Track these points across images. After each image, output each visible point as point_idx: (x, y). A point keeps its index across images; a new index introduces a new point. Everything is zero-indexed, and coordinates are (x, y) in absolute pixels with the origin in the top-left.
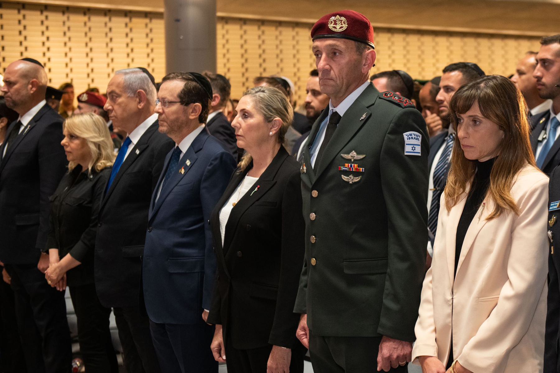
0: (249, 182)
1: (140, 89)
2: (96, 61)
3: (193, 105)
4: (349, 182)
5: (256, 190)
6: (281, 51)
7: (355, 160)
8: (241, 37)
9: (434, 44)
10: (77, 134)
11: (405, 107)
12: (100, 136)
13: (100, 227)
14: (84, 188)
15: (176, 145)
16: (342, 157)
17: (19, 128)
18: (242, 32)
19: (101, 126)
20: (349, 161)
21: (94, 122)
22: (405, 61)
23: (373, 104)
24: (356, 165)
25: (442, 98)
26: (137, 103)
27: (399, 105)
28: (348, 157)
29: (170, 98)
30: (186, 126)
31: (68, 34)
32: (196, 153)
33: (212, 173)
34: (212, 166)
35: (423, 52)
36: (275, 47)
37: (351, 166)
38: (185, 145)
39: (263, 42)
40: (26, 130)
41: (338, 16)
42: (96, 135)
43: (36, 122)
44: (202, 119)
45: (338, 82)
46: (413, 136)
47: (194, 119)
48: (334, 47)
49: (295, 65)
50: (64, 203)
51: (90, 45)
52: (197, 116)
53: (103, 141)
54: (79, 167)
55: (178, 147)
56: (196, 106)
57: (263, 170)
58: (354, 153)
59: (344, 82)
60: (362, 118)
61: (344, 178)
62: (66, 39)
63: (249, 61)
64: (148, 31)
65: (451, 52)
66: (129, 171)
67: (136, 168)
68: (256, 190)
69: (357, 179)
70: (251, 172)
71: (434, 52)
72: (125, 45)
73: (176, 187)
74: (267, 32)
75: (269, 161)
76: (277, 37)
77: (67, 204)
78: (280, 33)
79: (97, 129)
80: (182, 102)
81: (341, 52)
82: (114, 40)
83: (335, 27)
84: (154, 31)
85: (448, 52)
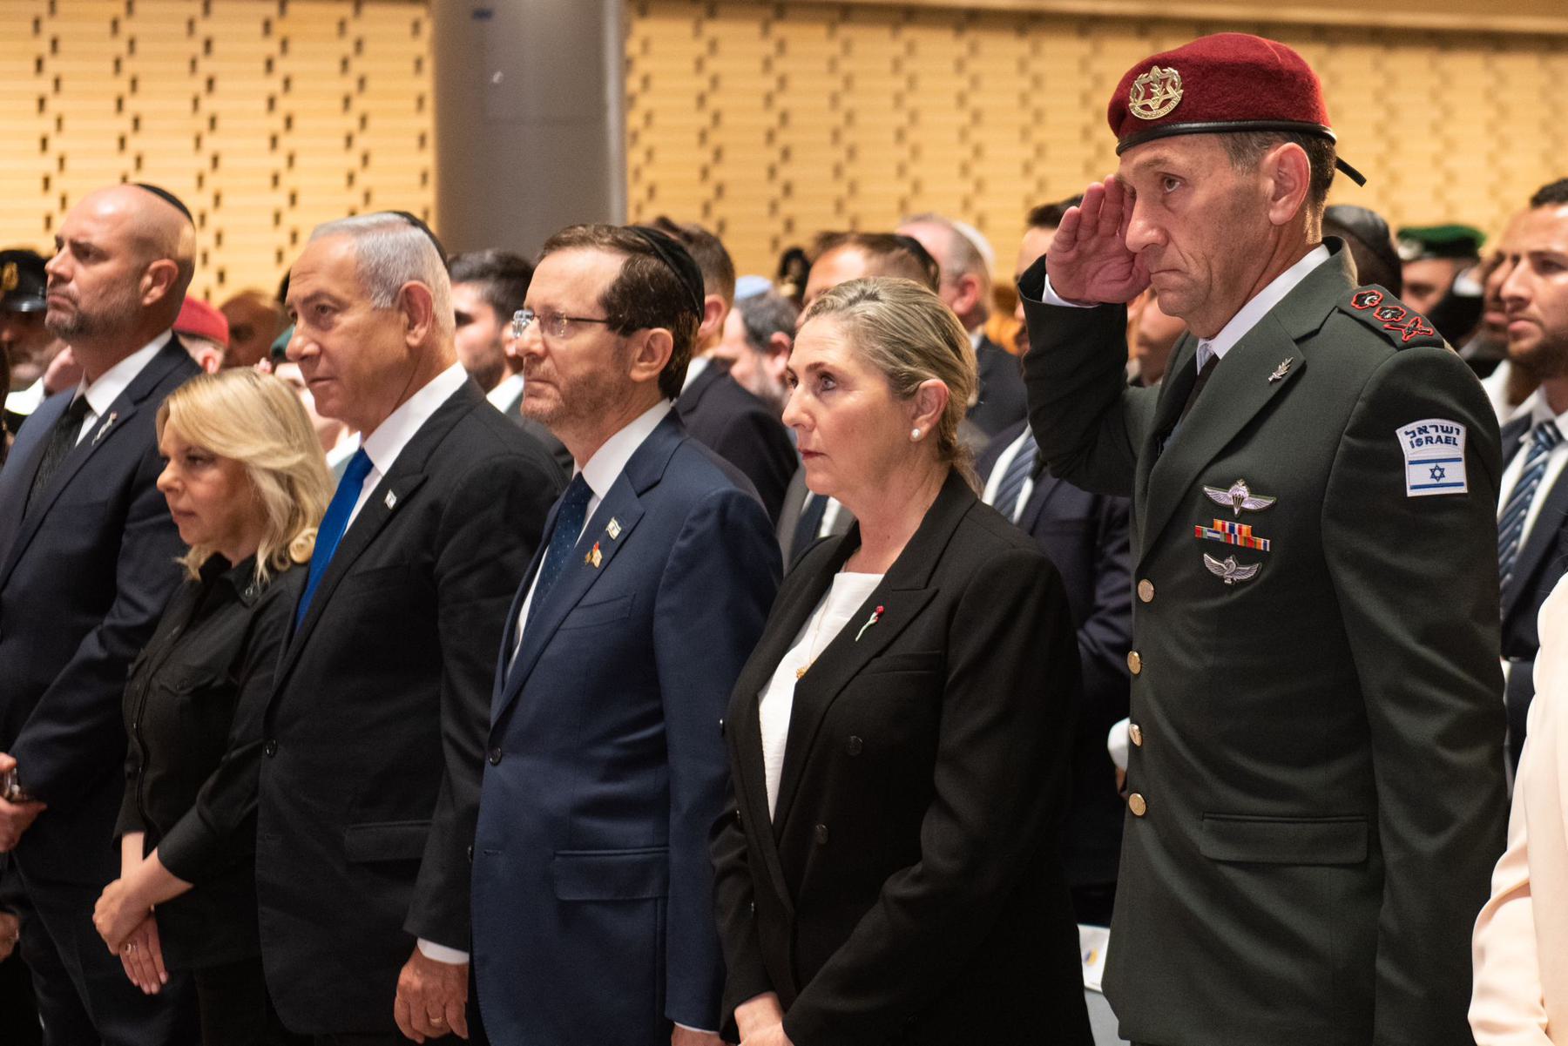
0: (851, 590)
1: (411, 278)
2: (303, 175)
3: (646, 334)
4: (1222, 579)
5: (872, 621)
6: (850, 117)
7: (1244, 512)
8: (699, 64)
9: (1434, 81)
10: (214, 448)
11: (1408, 346)
12: (292, 448)
13: (271, 756)
14: (226, 628)
15: (576, 470)
17: (79, 421)
18: (700, 47)
19: (285, 406)
20: (1225, 512)
21: (267, 399)
22: (1027, 118)
23: (1316, 332)
24: (1245, 527)
25: (1522, 291)
26: (401, 328)
27: (1388, 340)
28: (1223, 497)
29: (567, 306)
30: (617, 403)
31: (51, 66)
32: (639, 495)
33: (690, 561)
34: (691, 538)
35: (1392, 112)
36: (825, 102)
37: (1232, 529)
38: (602, 472)
39: (782, 82)
40: (103, 429)
41: (1156, 69)
42: (277, 445)
43: (136, 403)
44: (669, 381)
47: (648, 380)
49: (901, 170)
50: (155, 683)
51: (132, 105)
52: (655, 372)
53: (302, 465)
54: (217, 563)
55: (580, 474)
56: (654, 337)
57: (894, 556)
58: (1241, 490)
60: (1276, 375)
61: (1210, 561)
62: (45, 85)
63: (729, 155)
64: (347, 47)
65: (1503, 111)
66: (363, 566)
67: (383, 554)
68: (872, 621)
69: (1248, 572)
70: (856, 559)
71: (1436, 114)
72: (262, 105)
73: (575, 614)
74: (794, 47)
75: (913, 523)
76: (833, 64)
77: (162, 687)
78: (847, 47)
79: (278, 425)
80: (612, 323)
82: (220, 85)
84: (369, 47)
85: (1491, 113)
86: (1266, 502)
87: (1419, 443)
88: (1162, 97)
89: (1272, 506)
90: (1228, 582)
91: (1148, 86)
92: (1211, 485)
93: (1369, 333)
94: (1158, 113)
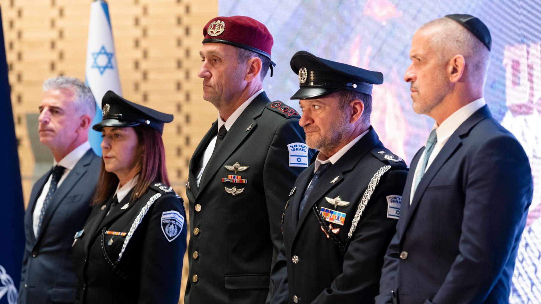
4: (232, 194)
11: (290, 118)
16: (226, 169)
20: (232, 172)
23: (260, 116)
24: (239, 176)
27: (283, 116)
41: (219, 21)
45: (217, 90)
46: (398, 200)
48: (214, 54)
58: (237, 164)
59: (224, 90)
60: (248, 129)
61: (228, 190)
69: (240, 191)
81: (220, 60)
83: (212, 32)
86: (245, 168)
87: (294, 150)
88: (219, 29)
89: (248, 169)
90: (234, 195)
91: (215, 26)
92: (228, 165)
93: (277, 115)
94: (215, 35)
